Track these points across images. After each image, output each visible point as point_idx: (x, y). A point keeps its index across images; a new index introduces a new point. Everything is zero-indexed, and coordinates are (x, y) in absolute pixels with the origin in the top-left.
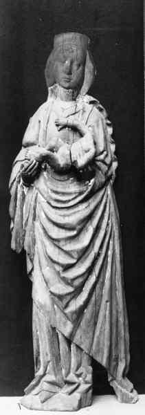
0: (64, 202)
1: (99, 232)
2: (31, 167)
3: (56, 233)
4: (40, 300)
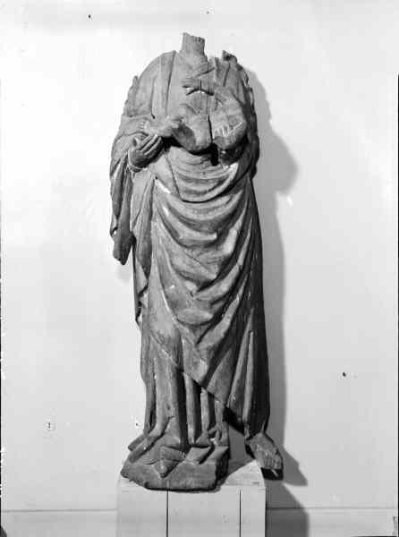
0: (198, 194)
1: (224, 240)
2: (147, 145)
3: (186, 233)
4: (162, 333)
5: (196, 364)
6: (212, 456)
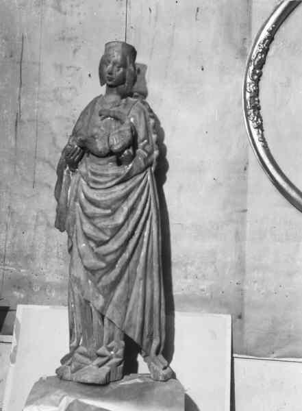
5: (97, 298)
6: (107, 364)
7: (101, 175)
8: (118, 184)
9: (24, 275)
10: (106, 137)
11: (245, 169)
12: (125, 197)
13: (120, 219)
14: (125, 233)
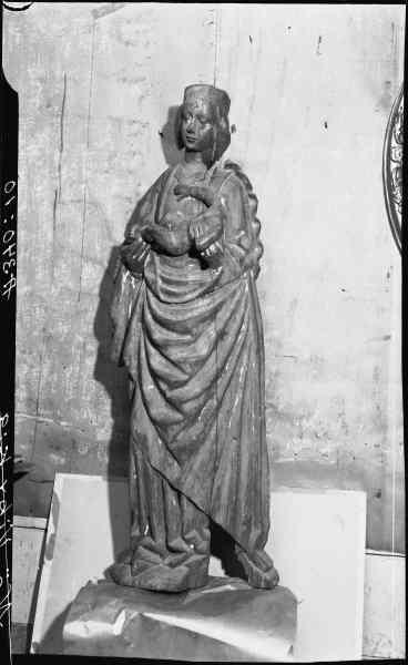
5: (170, 465)
7: (178, 283)
8: (202, 296)
9: (65, 429)
10: (185, 227)
11: (388, 276)
12: (212, 315)
13: (202, 348)
14: (210, 368)
